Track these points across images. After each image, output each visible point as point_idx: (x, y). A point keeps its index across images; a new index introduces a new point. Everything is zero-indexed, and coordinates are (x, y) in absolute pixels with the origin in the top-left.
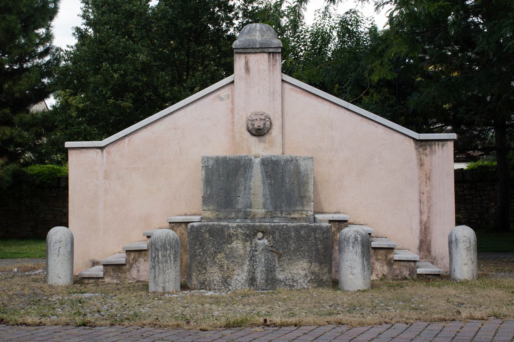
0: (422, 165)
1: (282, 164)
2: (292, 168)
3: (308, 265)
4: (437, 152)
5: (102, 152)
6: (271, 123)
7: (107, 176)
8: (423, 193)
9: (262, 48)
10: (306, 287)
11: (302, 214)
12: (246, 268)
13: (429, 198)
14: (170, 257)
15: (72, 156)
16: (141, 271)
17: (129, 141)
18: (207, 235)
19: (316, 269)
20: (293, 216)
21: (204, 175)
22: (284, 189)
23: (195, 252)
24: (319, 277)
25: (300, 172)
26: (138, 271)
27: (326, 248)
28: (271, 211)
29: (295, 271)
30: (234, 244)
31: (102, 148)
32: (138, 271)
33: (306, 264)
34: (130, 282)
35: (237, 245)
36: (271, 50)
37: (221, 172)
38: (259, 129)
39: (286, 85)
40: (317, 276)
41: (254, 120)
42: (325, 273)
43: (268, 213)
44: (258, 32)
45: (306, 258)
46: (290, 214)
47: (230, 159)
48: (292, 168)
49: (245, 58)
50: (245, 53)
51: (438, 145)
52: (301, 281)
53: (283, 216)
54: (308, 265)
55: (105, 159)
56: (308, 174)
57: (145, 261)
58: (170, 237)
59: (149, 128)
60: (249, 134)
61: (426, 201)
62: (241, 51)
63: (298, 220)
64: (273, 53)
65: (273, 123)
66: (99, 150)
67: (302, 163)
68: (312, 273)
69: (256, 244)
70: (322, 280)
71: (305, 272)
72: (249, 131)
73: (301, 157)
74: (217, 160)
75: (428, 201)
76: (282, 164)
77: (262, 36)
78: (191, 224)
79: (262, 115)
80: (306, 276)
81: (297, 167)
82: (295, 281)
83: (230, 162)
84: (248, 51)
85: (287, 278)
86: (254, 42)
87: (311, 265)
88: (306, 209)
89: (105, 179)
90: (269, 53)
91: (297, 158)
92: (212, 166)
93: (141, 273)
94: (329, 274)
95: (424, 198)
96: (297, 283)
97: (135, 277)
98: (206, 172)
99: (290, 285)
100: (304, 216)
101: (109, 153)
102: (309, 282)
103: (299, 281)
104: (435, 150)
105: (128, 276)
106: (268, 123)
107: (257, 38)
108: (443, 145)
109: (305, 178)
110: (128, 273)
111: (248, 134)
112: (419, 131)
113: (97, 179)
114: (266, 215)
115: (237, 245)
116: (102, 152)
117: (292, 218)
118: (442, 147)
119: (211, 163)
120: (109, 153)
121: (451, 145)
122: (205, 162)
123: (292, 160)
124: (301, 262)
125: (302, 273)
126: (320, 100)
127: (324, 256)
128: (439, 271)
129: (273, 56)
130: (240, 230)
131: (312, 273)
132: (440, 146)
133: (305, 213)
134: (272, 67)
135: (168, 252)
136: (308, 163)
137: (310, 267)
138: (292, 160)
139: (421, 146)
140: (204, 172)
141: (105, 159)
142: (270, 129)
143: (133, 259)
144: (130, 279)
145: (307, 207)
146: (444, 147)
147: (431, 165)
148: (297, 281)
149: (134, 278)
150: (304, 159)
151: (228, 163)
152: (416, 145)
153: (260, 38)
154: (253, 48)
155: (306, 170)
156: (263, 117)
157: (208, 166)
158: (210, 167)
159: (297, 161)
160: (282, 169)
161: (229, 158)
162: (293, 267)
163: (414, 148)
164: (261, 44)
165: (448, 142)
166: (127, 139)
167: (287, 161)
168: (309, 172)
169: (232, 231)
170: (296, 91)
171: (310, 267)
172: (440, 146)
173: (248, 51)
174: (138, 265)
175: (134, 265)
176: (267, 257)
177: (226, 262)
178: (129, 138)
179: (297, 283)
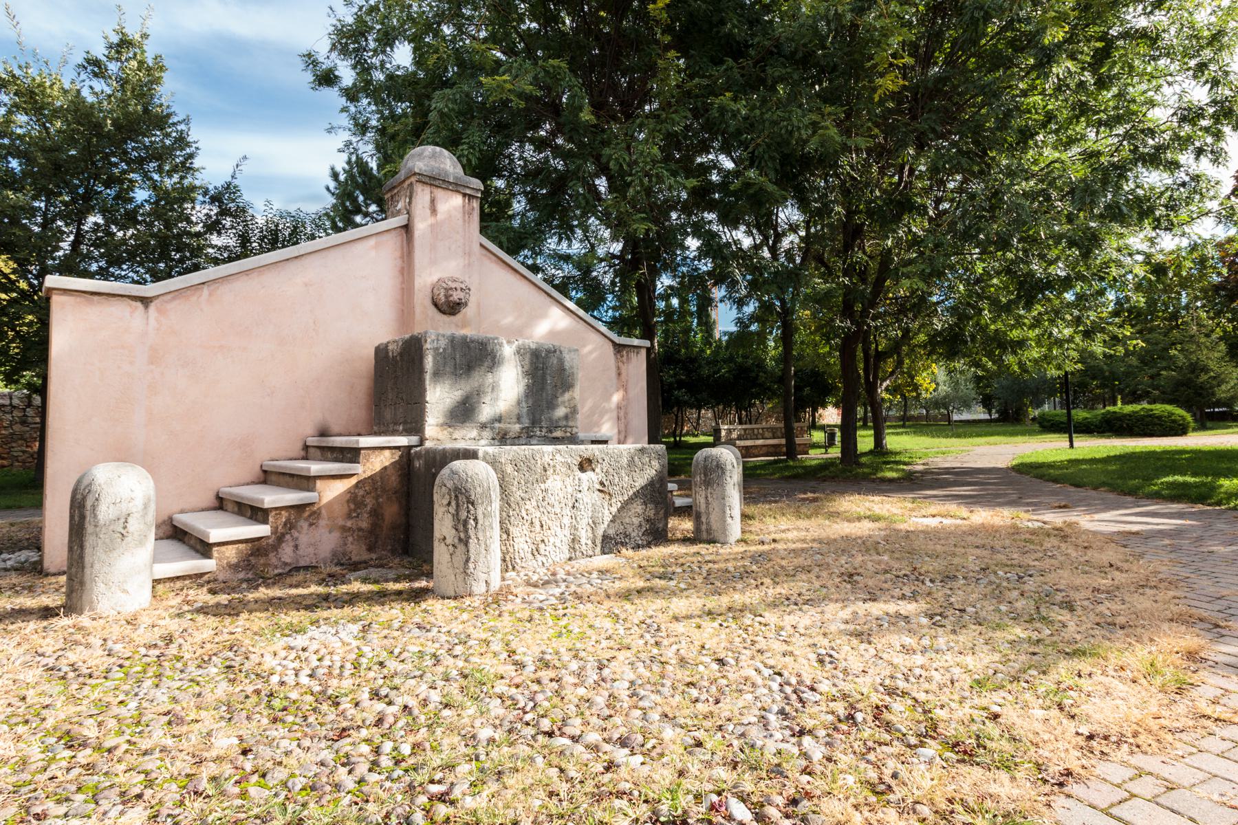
0: (619, 374)
7: (155, 357)
9: (456, 184)
13: (626, 413)
15: (58, 304)
16: (302, 547)
17: (210, 295)
19: (651, 513)
26: (296, 547)
29: (627, 520)
31: (145, 301)
32: (296, 547)
34: (276, 572)
36: (468, 191)
57: (311, 525)
60: (435, 310)
62: (427, 180)
64: (470, 196)
66: (139, 304)
67: (567, 357)
72: (436, 305)
80: (640, 526)
84: (437, 183)
86: (446, 173)
88: (571, 424)
90: (464, 195)
93: (300, 552)
95: (622, 414)
97: (288, 561)
105: (274, 561)
110: (272, 555)
111: (432, 311)
112: (620, 334)
121: (644, 352)
125: (636, 521)
130: (558, 457)
141: (152, 321)
143: (285, 524)
144: (276, 567)
149: (286, 564)
150: (570, 351)
155: (572, 367)
157: (437, 349)
167: (548, 351)
169: (547, 459)
173: (437, 183)
174: (296, 534)
175: (288, 537)
178: (212, 288)
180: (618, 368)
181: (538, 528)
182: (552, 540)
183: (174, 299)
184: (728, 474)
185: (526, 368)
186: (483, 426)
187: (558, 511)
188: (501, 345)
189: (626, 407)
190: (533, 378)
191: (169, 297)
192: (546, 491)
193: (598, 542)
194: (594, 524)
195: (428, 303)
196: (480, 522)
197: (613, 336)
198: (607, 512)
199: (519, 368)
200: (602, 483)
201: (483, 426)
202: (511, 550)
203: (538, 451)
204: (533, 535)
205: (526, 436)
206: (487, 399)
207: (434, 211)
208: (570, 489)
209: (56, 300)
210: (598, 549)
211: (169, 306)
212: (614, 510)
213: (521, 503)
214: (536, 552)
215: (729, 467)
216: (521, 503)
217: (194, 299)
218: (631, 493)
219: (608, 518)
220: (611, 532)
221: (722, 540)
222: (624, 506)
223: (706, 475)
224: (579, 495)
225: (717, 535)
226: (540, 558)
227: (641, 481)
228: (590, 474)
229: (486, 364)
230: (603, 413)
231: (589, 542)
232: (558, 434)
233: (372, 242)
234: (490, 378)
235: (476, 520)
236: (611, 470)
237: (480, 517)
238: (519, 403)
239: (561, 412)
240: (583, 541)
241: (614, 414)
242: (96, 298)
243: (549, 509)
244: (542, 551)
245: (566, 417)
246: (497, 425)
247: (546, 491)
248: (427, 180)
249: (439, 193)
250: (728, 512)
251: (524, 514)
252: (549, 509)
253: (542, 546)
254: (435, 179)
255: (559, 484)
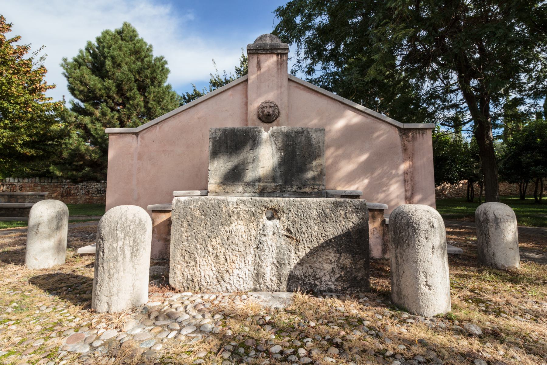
1: (293, 135)
2: (303, 140)
3: (335, 256)
4: (418, 139)
5: (137, 137)
6: (279, 113)
7: (140, 157)
8: (407, 174)
9: (271, 49)
10: (333, 287)
11: (314, 189)
12: (250, 258)
14: (123, 250)
17: (160, 129)
18: (197, 213)
20: (304, 190)
21: (211, 147)
22: (294, 162)
23: (182, 236)
24: (351, 274)
25: (311, 145)
27: (360, 232)
28: (281, 185)
30: (233, 226)
31: (137, 134)
33: (332, 255)
35: (238, 227)
36: (279, 51)
37: (229, 144)
38: (268, 115)
39: (291, 83)
40: (348, 272)
41: (264, 107)
42: (360, 268)
43: (278, 187)
44: (268, 38)
45: (333, 246)
46: (300, 188)
47: (239, 131)
48: (303, 140)
49: (258, 58)
50: (257, 54)
51: (419, 133)
52: (327, 278)
53: (294, 190)
54: (335, 256)
55: (139, 143)
56: (319, 147)
58: (126, 219)
59: (177, 117)
60: (260, 121)
61: (410, 180)
62: (254, 52)
63: (310, 195)
65: (281, 112)
66: (135, 136)
67: (314, 135)
68: (342, 268)
69: (264, 225)
70: (355, 278)
71: (332, 266)
73: (312, 129)
74: (225, 132)
75: (411, 180)
76: (293, 135)
77: (272, 41)
78: (176, 198)
79: (271, 103)
80: (333, 271)
81: (309, 138)
82: (317, 279)
83: (238, 133)
84: (260, 52)
85: (307, 274)
86: (265, 45)
87: (341, 256)
89: (138, 159)
90: (278, 54)
91: (309, 130)
92: (220, 138)
94: (365, 270)
95: (408, 177)
96: (321, 282)
98: (213, 143)
99: (310, 283)
100: (316, 190)
101: (142, 138)
102: (337, 280)
103: (323, 279)
104: (417, 137)
106: (276, 110)
107: (267, 42)
108: (423, 134)
109: (316, 150)
112: (404, 122)
113: (132, 160)
114: (276, 189)
115: (238, 227)
116: (137, 137)
117: (303, 193)
118: (422, 135)
119: (219, 134)
120: (142, 138)
122: (213, 134)
123: (303, 132)
124: (326, 253)
125: (328, 267)
126: (319, 95)
127: (357, 244)
128: (459, 251)
129: (281, 57)
130: (242, 206)
131: (342, 268)
132: (421, 134)
133: (316, 187)
134: (279, 66)
135: (120, 243)
136: (320, 135)
137: (339, 259)
138: (303, 132)
139: (404, 134)
140: (211, 144)
142: (277, 117)
145: (319, 181)
146: (424, 135)
147: (413, 150)
148: (320, 278)
150: (316, 131)
151: (236, 135)
152: (400, 132)
153: (270, 42)
154: (264, 49)
156: (272, 105)
157: (215, 138)
158: (218, 138)
159: (308, 132)
160: (293, 141)
161: (237, 130)
162: (315, 259)
163: (398, 136)
164: (271, 46)
165: (427, 131)
166: (158, 126)
168: (321, 144)
169: (231, 207)
170: (300, 88)
171: (339, 259)
172: (421, 134)
176: (279, 245)
177: (223, 250)
179: (321, 282)
180: (404, 145)
181: (222, 260)
182: (236, 272)
183: (146, 132)
184: (422, 234)
185: (280, 145)
186: (248, 184)
187: (242, 249)
188: (260, 131)
189: (412, 173)
190: (285, 152)
191: (145, 131)
192: (231, 232)
193: (284, 279)
194: (279, 264)
195: (255, 118)
196: (106, 254)
197: (401, 125)
198: (293, 255)
199: (274, 146)
200: (288, 230)
201: (248, 184)
202: (198, 274)
203: (223, 201)
204: (218, 266)
205: (281, 191)
206: (250, 167)
207: (259, 67)
208: (253, 233)
209: (111, 137)
210: (284, 286)
211: (145, 135)
212: (302, 254)
213: (207, 239)
214: (220, 279)
215: (424, 226)
216: (207, 239)
217: (154, 131)
218: (322, 241)
219: (294, 261)
220: (298, 273)
221: (414, 310)
222: (314, 253)
223: (395, 233)
224: (263, 239)
225: (409, 303)
226: (224, 285)
227: (333, 231)
228: (276, 222)
229: (248, 145)
230: (391, 177)
231: (274, 279)
232: (307, 190)
233: (230, 92)
234: (251, 154)
235: (103, 252)
236: (298, 220)
237: (106, 251)
238: (274, 169)
239: (310, 174)
240: (268, 276)
241: (401, 178)
242: (121, 135)
243: (234, 247)
244: (227, 280)
245: (314, 178)
246: (257, 184)
247: (231, 232)
248: (254, 52)
249: (263, 57)
250: (422, 278)
251: (210, 249)
252: (234, 247)
253: (226, 276)
254: (258, 50)
255: (243, 228)
